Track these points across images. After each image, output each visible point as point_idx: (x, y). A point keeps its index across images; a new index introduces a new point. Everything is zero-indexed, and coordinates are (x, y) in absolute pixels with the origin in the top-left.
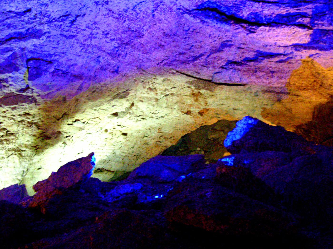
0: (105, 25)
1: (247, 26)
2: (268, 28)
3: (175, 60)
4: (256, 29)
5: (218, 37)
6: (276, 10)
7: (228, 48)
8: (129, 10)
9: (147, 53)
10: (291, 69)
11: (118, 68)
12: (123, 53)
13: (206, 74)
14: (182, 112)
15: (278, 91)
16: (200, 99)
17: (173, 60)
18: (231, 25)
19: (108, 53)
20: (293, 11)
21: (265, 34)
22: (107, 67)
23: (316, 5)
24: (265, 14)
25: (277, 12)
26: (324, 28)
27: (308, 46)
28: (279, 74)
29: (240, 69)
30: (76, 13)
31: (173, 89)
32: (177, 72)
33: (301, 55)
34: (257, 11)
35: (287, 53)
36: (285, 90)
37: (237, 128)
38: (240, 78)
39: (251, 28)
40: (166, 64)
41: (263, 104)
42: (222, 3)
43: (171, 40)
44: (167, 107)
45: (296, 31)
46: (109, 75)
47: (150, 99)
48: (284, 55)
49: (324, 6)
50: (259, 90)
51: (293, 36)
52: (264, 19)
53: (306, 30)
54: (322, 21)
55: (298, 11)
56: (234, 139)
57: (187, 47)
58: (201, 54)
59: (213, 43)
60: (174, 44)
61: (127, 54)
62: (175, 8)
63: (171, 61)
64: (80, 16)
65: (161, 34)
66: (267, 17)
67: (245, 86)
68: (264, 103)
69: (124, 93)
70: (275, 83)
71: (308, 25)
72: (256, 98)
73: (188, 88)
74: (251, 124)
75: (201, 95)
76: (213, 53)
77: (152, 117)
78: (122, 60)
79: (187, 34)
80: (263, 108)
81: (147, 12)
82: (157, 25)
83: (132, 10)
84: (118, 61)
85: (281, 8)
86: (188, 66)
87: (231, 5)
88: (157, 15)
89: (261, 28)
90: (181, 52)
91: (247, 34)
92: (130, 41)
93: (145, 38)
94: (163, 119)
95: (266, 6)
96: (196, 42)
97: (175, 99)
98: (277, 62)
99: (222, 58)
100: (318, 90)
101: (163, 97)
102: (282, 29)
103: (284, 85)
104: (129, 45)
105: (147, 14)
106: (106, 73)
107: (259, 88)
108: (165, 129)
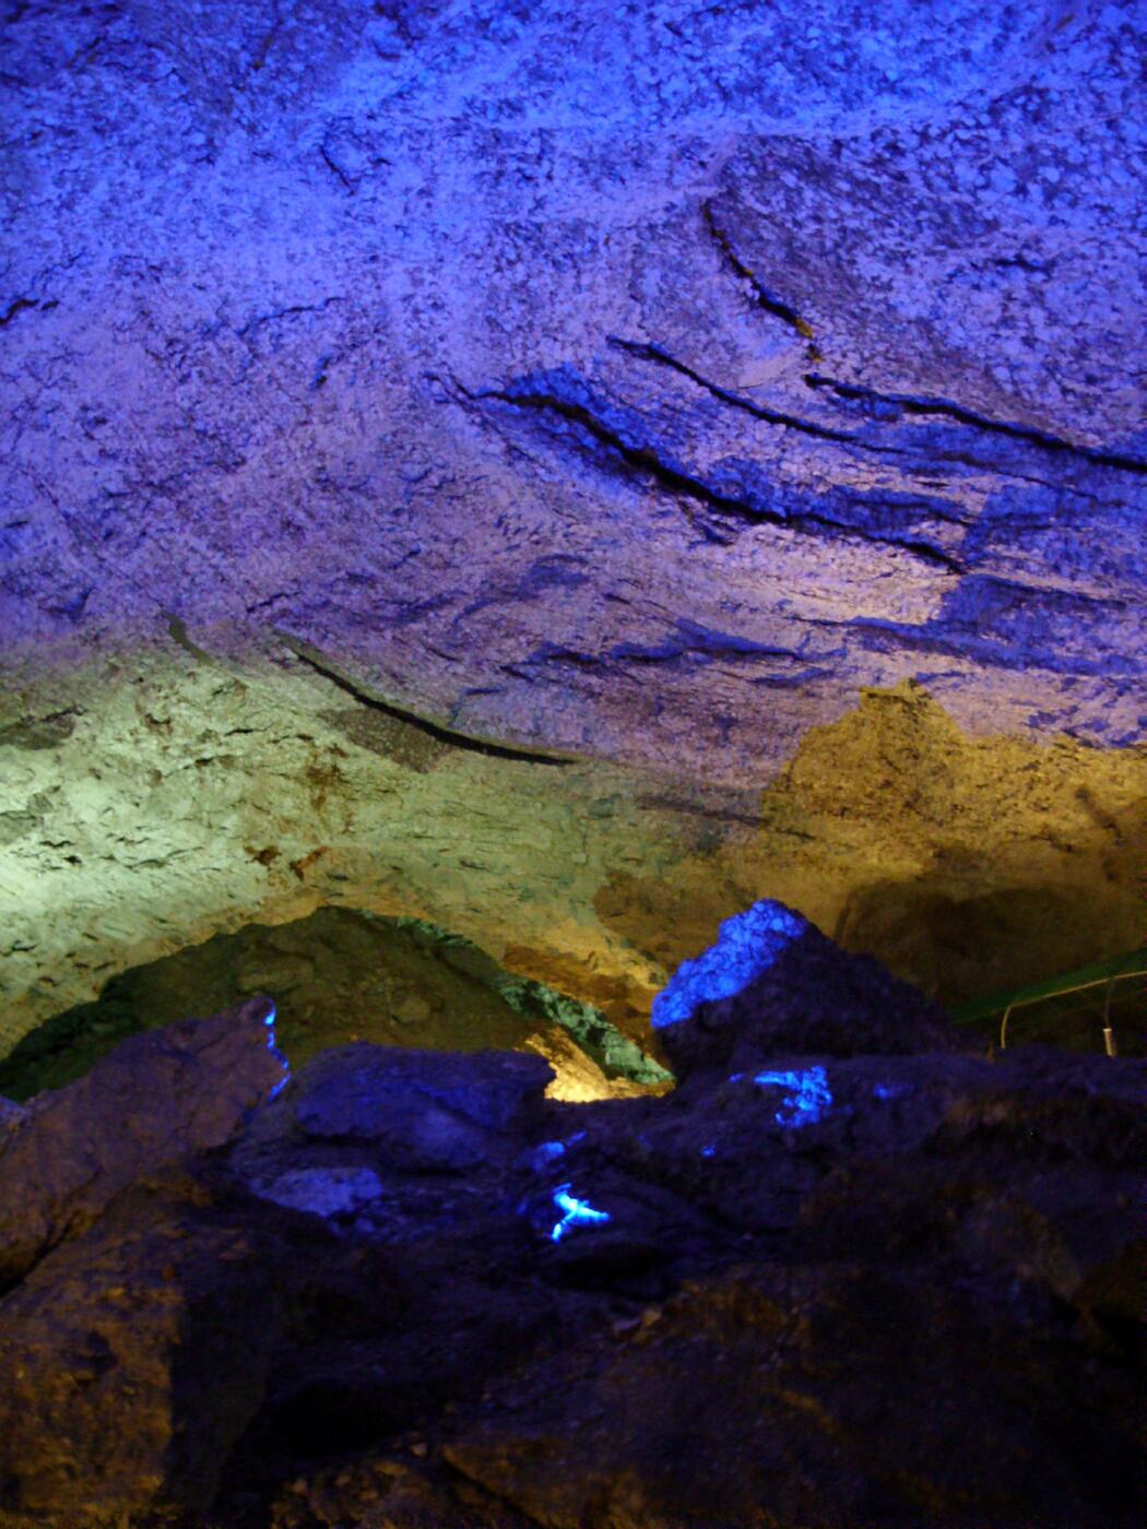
0: (107, 374)
1: (704, 511)
2: (789, 534)
3: (327, 603)
4: (737, 532)
5: (535, 532)
6: (836, 469)
7: (561, 590)
8: (224, 331)
9: (225, 549)
10: (803, 720)
11: (85, 596)
12: (129, 528)
13: (429, 690)
14: (249, 850)
15: (712, 808)
16: (332, 799)
17: (318, 600)
18: (645, 492)
19: (67, 516)
20: (902, 485)
21: (768, 559)
22: (37, 580)
23: (1010, 481)
24: (788, 472)
25: (837, 476)
26: (1023, 577)
27: (922, 640)
28: (751, 736)
29: (597, 690)
30: (23, 285)
31: (238, 738)
32: (302, 659)
33: (881, 670)
34: (758, 457)
35: (813, 652)
36: (747, 808)
37: (724, 949)
38: (586, 731)
39: (716, 523)
40: (284, 613)
41: (622, 854)
42: (618, 393)
43: (337, 509)
44: (192, 818)
45: (896, 569)
46: (38, 623)
47: (127, 768)
48: (797, 657)
49: (1042, 493)
50: (624, 792)
51: (877, 587)
52: (779, 494)
53: (942, 570)
54: (1021, 548)
55: (926, 492)
56: (710, 995)
57: (392, 552)
58: (440, 596)
59: (504, 555)
60: (346, 529)
61: (144, 534)
62: (415, 368)
63: (306, 606)
64: (32, 304)
65: (306, 474)
66: (794, 490)
67: (567, 767)
68: (627, 853)
69: (53, 725)
70: (728, 771)
71: (953, 555)
72: (596, 824)
73: (299, 742)
74: (782, 935)
75: (340, 780)
76: (493, 601)
77: (111, 858)
78: (113, 560)
79: (410, 494)
80: (611, 873)
81: (297, 358)
82: (310, 428)
83: (241, 334)
84: (94, 563)
85: (863, 466)
86: (372, 641)
87: (655, 406)
88: (337, 381)
89: (761, 528)
90: (358, 571)
91: (692, 545)
92: (180, 476)
93: (244, 475)
94: (156, 871)
95: (800, 444)
96: (436, 539)
97: (237, 783)
98: (758, 682)
99: (526, 628)
100: (895, 824)
101: (186, 768)
102: (845, 552)
103: (763, 785)
104: (170, 493)
105: (293, 368)
106: (24, 611)
107: (626, 786)
108: (113, 924)
